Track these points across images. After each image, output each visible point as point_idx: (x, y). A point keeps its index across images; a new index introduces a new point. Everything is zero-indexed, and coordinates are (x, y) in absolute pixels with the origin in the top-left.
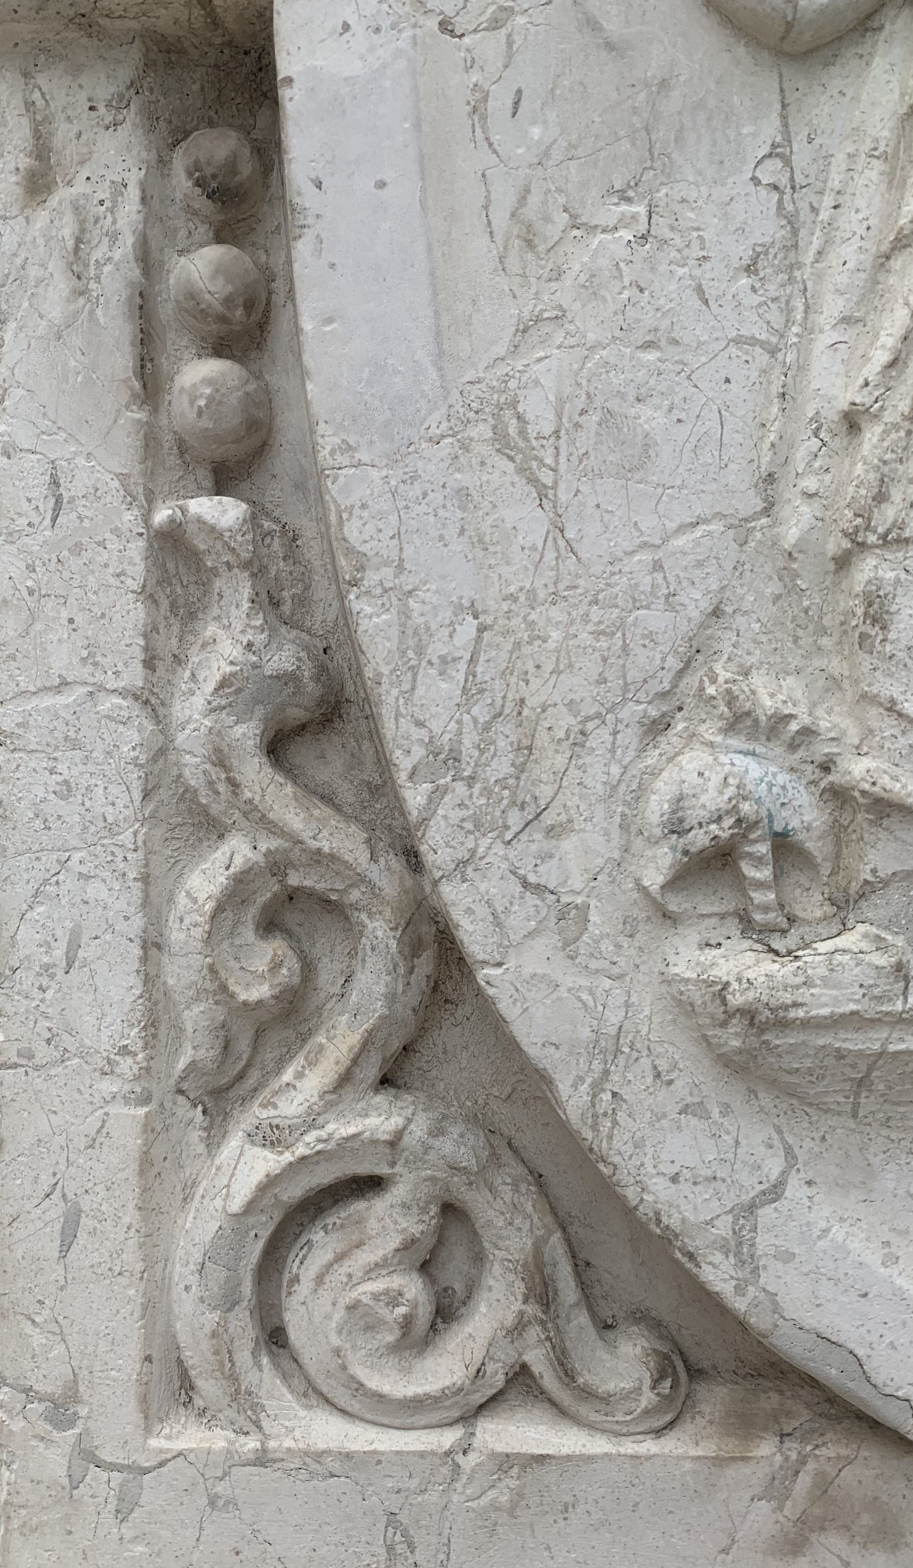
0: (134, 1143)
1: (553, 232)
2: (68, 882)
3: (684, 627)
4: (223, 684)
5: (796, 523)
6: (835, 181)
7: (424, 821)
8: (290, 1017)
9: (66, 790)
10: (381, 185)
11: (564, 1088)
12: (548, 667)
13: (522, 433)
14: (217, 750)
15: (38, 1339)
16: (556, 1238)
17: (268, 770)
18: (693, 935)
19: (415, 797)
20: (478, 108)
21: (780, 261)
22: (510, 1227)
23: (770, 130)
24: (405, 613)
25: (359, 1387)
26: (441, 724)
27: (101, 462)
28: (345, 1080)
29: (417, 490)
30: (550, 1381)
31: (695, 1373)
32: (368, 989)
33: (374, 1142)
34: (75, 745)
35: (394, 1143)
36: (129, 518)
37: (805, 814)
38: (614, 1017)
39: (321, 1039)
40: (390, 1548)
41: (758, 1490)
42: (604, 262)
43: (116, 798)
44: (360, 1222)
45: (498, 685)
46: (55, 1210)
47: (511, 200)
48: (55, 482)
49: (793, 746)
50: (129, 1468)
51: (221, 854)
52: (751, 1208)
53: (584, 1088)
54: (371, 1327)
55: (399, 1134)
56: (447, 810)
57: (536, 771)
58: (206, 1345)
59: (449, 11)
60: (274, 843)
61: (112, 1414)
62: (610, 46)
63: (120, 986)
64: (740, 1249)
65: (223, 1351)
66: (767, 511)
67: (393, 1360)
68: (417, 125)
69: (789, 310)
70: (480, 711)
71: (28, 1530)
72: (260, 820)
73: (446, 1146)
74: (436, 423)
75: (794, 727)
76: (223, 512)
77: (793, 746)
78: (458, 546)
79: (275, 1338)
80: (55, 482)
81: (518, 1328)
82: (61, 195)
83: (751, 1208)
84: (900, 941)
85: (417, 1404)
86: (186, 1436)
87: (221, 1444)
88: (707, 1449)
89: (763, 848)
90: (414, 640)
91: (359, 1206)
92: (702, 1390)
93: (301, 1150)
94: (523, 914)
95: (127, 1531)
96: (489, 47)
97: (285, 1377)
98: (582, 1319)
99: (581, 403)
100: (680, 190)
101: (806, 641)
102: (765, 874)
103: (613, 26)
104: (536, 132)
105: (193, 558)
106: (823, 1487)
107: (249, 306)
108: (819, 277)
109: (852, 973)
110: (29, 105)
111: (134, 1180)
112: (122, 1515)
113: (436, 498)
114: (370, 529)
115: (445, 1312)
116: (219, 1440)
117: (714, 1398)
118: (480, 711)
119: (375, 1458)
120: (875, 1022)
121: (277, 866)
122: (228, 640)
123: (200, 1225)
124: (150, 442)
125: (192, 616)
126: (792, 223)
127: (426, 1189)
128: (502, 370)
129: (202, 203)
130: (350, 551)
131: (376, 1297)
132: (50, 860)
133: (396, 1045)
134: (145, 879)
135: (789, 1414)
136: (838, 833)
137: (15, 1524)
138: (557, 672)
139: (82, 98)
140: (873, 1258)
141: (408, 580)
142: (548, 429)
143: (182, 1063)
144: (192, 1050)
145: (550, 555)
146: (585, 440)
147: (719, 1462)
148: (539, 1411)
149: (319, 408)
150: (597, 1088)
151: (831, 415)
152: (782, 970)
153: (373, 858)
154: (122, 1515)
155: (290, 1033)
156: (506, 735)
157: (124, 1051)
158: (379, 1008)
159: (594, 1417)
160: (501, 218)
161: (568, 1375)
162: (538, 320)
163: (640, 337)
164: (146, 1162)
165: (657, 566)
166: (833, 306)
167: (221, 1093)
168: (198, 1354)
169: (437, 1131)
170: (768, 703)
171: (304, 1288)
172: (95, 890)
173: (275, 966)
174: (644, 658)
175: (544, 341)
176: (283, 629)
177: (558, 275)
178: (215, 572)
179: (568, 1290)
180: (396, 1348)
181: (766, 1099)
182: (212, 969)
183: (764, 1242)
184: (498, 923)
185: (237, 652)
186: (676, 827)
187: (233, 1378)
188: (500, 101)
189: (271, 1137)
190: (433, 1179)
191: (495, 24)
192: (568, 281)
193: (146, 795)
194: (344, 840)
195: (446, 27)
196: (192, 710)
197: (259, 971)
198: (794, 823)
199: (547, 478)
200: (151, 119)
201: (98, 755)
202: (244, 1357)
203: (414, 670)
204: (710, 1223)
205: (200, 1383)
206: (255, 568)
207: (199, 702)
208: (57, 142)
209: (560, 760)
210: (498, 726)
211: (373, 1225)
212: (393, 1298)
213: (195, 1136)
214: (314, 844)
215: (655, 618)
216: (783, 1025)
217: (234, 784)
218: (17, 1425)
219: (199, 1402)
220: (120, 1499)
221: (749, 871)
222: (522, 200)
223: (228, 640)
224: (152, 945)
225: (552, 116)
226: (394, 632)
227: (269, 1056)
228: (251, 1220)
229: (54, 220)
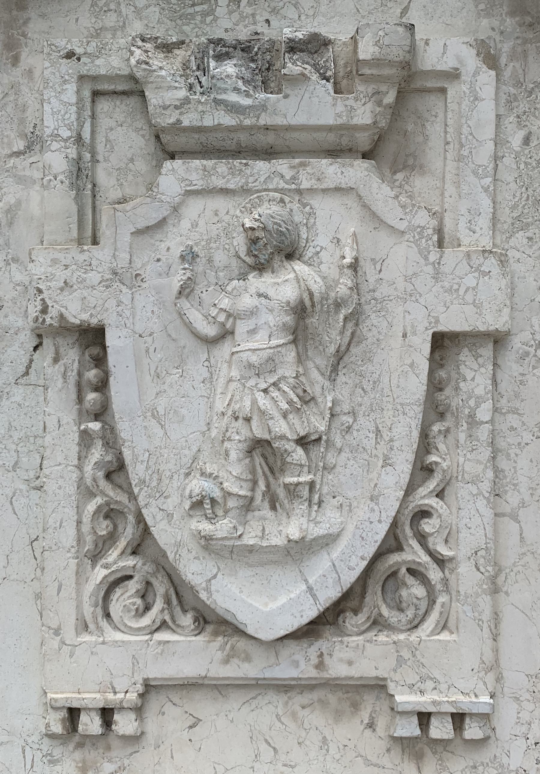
0: (75, 568)
1: (163, 375)
2: (60, 508)
3: (192, 454)
4: (95, 464)
5: (214, 433)
6: (219, 366)
7: (138, 496)
8: (112, 538)
9: (60, 488)
10: (127, 367)
11: (169, 554)
12: (164, 462)
13: (158, 414)
14: (94, 479)
15: (52, 615)
16: (172, 589)
17: (105, 482)
18: (195, 520)
19: (136, 490)
20: (147, 351)
21: (210, 380)
22: (161, 587)
23: (206, 356)
24: (134, 451)
25: (126, 625)
26: (141, 474)
27: (69, 417)
28: (123, 553)
29: (136, 426)
30: (170, 624)
31: (206, 622)
32: (128, 533)
33: (129, 567)
34: (62, 477)
35: (134, 567)
36: (75, 428)
37: (217, 494)
38: (179, 538)
39: (118, 543)
40: (133, 664)
41: (218, 648)
42: (173, 381)
43: (72, 489)
44: (127, 586)
45: (154, 466)
46: (56, 584)
47: (155, 369)
48: (59, 421)
49: (214, 479)
50: (72, 645)
51: (95, 501)
52: (210, 580)
53: (173, 554)
54: (129, 611)
55: (135, 565)
56: (143, 493)
57: (162, 484)
58: (91, 616)
59: (141, 333)
60: (107, 499)
61: (69, 633)
62: (173, 340)
63: (72, 532)
64: (208, 590)
65: (95, 618)
66: (208, 430)
67: (134, 619)
68: (135, 355)
69: (211, 390)
70: (150, 472)
71: (49, 660)
72: (103, 493)
73: (146, 568)
74: (139, 413)
75: (214, 475)
76: (95, 426)
77: (214, 479)
78: (145, 437)
79: (108, 615)
80: (59, 421)
81: (163, 610)
82: (61, 362)
83: (210, 580)
84: (235, 521)
85: (139, 629)
86: (86, 638)
87: (94, 639)
88: (207, 639)
89: (208, 501)
90: (135, 457)
91: (127, 582)
92: (207, 626)
93: (113, 569)
94: (160, 515)
95: (72, 660)
96: (149, 339)
97: (110, 624)
98: (178, 609)
99: (170, 408)
100: (188, 367)
101: (218, 457)
102: (209, 506)
103: (174, 336)
104: (159, 356)
105: (90, 435)
106: (233, 648)
107: (102, 382)
108: (217, 384)
109: (225, 528)
110: (55, 344)
111: (74, 577)
112: (71, 656)
113: (140, 428)
114: (126, 434)
115: (147, 608)
116: (94, 638)
117: (209, 628)
118: (150, 472)
119: (130, 642)
120: (231, 538)
121: (108, 504)
122: (97, 453)
123: (89, 588)
124: (80, 412)
125: (89, 447)
126: (211, 374)
127: (142, 578)
128: (153, 402)
129: (91, 360)
130: (122, 439)
131: (130, 603)
132: (56, 503)
133: (135, 544)
134: (77, 507)
135: (227, 631)
136: (224, 497)
137: (46, 659)
138: (166, 463)
139: (66, 343)
140: (237, 591)
141: (134, 445)
142: (163, 414)
143: (86, 549)
144: (89, 546)
145: (164, 439)
146: (171, 416)
147: (209, 642)
148: (169, 631)
149: (115, 411)
150: (176, 554)
151: (219, 412)
152: (211, 527)
153: (129, 502)
154: (71, 656)
155: (112, 542)
156: (155, 476)
157: (72, 547)
158: (131, 536)
159: (181, 632)
160: (152, 372)
161: (174, 621)
162: (160, 392)
163: (181, 396)
164: (77, 573)
165: (187, 441)
166: (219, 390)
167: (95, 557)
168: (89, 618)
169: (144, 564)
170: (209, 470)
171: (114, 602)
172: (66, 510)
173: (107, 527)
174: (184, 460)
175: (162, 396)
176: (110, 449)
177: (164, 383)
178: (94, 438)
179: (175, 601)
180: (135, 616)
181: (213, 555)
182: (93, 528)
183: (213, 588)
184: (154, 518)
185: (99, 456)
186: (191, 497)
187: (97, 624)
188: (151, 350)
189: (106, 566)
190: (143, 576)
191: (150, 335)
192: (166, 384)
193: (78, 488)
194: (123, 498)
195: (140, 336)
196: (88, 469)
197: (104, 528)
198: (215, 496)
199: (163, 423)
200: (81, 345)
201: (67, 479)
202: (100, 619)
203: (136, 463)
204: (201, 584)
205: (90, 625)
206: (103, 438)
207: (90, 467)
208: (60, 352)
209: (168, 482)
210: (154, 475)
211: (130, 587)
212: (134, 604)
213: (89, 566)
214: (116, 499)
215: (187, 452)
216: (212, 539)
217: (98, 486)
218: (47, 635)
219: (89, 630)
220: (71, 653)
221: (205, 506)
222: (157, 369)
223: (97, 453)
224: (79, 522)
225: (162, 352)
226: (131, 455)
227: (106, 547)
228: (101, 585)
229: (59, 367)
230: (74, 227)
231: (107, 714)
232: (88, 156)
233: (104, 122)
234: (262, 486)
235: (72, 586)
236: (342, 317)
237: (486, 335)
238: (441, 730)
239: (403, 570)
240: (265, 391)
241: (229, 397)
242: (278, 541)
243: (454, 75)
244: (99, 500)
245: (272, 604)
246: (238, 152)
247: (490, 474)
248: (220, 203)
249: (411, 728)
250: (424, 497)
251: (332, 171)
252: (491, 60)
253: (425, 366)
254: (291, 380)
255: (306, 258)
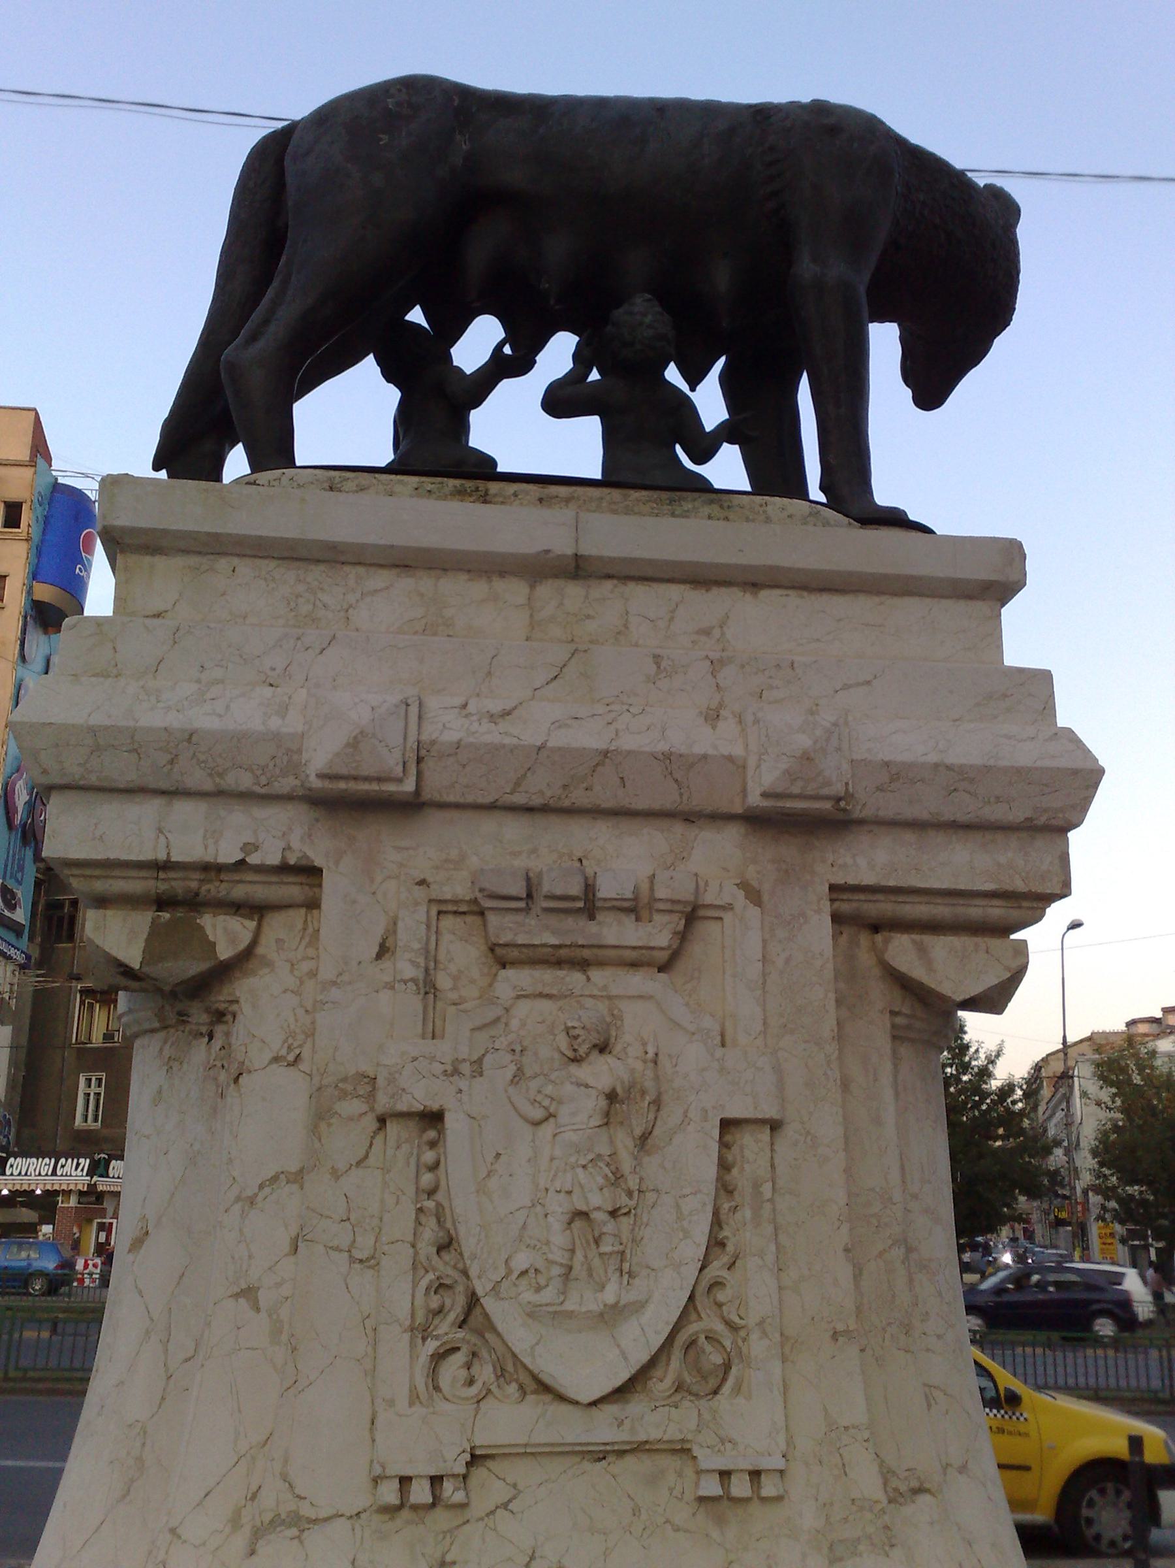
72: (434, 1270)
79: (437, 1388)
85: (467, 1399)
230: (420, 1024)
231: (436, 1481)
232: (432, 964)
233: (446, 937)
234: (579, 1255)
235: (401, 1362)
236: (647, 1103)
237: (763, 1122)
238: (740, 1487)
239: (702, 1337)
240: (584, 1167)
241: (552, 1173)
242: (593, 1307)
243: (729, 907)
244: (431, 1276)
245: (589, 1366)
246: (559, 963)
247: (773, 1248)
248: (546, 1005)
249: (712, 1487)
250: (716, 1269)
251: (638, 981)
252: (754, 896)
253: (715, 1147)
254: (607, 1158)
255: (614, 1053)
